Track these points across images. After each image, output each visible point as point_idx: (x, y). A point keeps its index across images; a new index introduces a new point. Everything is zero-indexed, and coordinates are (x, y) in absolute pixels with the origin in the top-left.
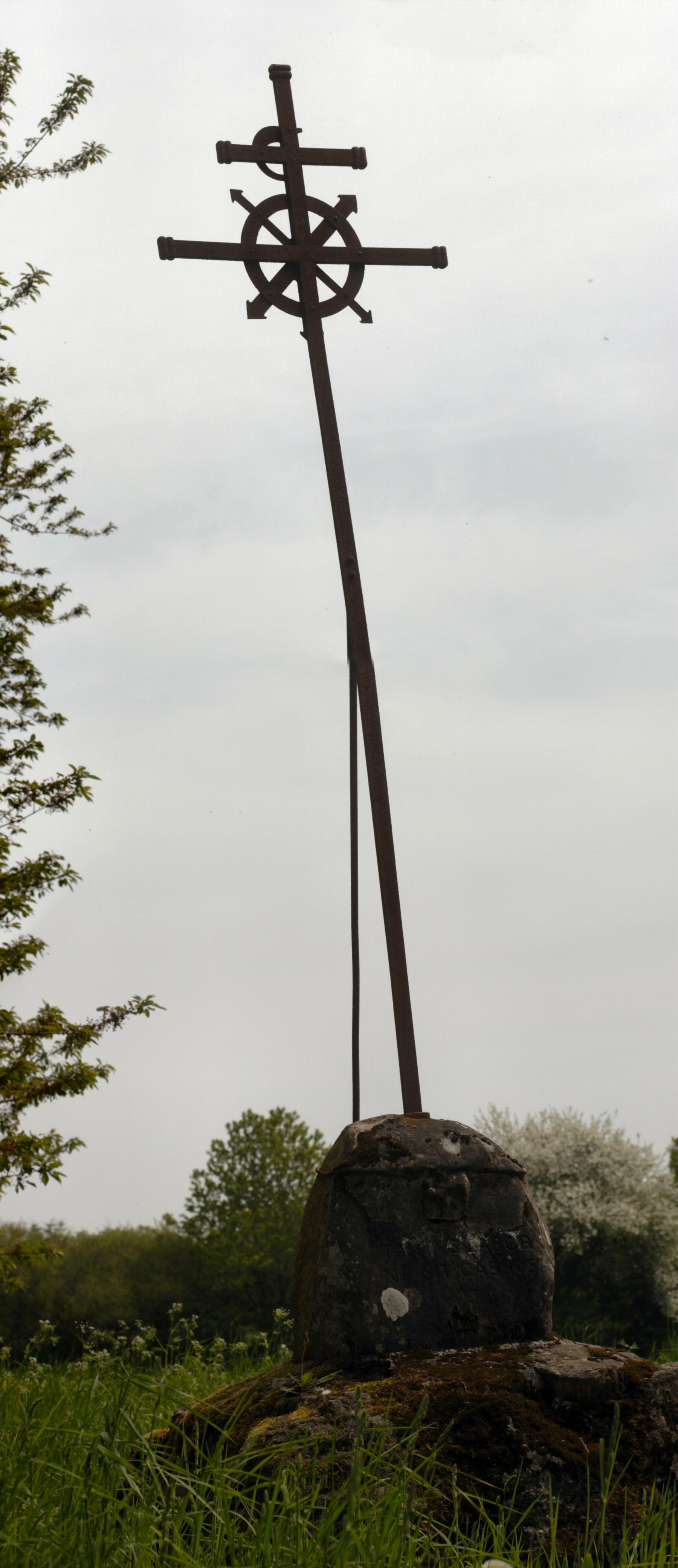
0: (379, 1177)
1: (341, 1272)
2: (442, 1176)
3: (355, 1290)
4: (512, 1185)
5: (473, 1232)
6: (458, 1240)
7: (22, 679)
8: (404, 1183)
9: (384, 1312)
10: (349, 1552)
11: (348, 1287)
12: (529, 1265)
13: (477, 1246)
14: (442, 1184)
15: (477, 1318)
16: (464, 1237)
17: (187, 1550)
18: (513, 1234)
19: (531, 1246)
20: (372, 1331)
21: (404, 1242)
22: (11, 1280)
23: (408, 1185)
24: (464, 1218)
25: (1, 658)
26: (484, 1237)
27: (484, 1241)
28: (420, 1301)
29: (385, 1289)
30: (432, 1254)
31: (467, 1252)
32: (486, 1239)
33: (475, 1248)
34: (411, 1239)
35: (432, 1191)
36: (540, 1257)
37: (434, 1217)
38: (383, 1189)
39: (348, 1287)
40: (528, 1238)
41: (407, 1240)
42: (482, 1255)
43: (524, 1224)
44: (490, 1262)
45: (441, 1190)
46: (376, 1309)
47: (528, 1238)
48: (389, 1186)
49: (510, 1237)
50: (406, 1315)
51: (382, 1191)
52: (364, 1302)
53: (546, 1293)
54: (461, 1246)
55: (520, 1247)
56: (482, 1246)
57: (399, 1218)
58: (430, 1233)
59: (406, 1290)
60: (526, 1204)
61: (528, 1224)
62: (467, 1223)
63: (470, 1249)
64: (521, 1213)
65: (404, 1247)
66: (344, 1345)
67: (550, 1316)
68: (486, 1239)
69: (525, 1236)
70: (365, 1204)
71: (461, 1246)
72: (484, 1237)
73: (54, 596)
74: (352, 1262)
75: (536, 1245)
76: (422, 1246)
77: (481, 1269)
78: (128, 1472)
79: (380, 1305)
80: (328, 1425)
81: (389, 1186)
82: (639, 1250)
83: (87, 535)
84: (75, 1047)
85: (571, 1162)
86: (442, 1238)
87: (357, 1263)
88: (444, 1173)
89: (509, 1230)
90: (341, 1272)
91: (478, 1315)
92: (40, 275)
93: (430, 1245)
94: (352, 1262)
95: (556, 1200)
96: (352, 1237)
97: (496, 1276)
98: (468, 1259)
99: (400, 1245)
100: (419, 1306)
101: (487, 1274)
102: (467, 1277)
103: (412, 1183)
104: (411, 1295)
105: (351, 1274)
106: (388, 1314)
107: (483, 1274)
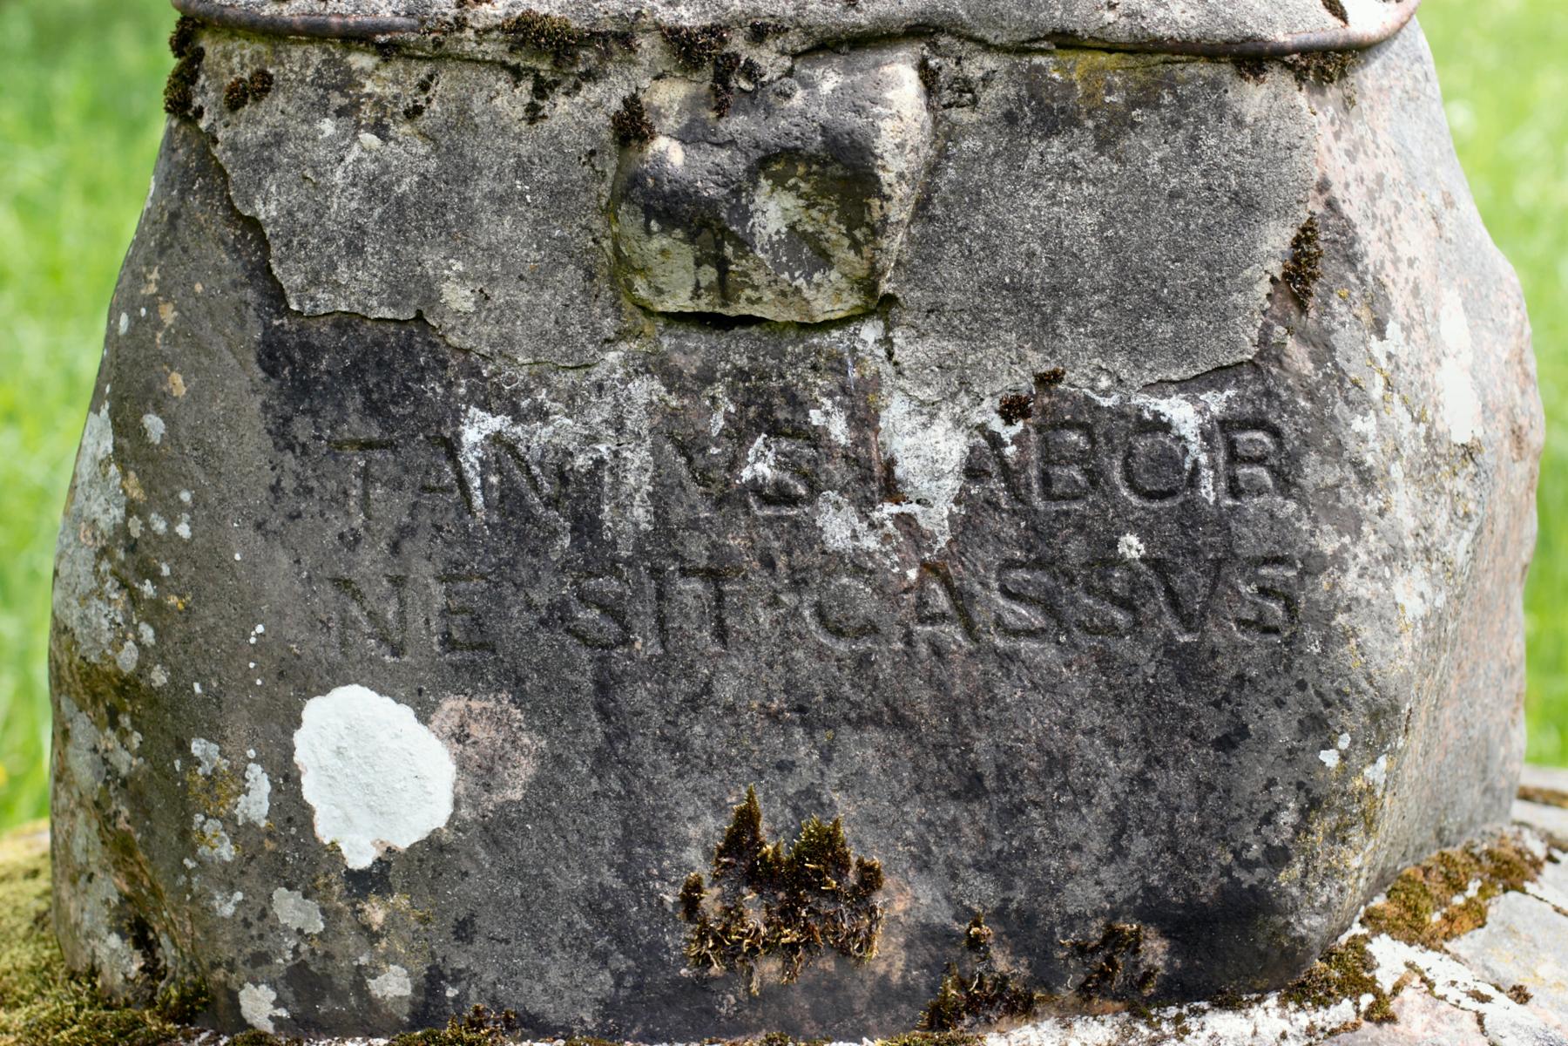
0: (361, 61)
1: (105, 566)
2: (751, 71)
3: (159, 677)
4: (1239, 123)
5: (927, 394)
6: (815, 438)
7: (798, 577)
8: (511, 100)
9: (307, 812)
10: (1222, 454)
11: (128, 658)
12: (1248, 590)
13: (937, 476)
14: (736, 124)
15: (870, 879)
16: (864, 420)
17: (1487, 749)
18: (1181, 413)
19: (1286, 483)
20: (228, 910)
21: (471, 435)
22: (947, 112)
23: (533, 114)
24: (881, 306)
25: (6, 115)
26: (997, 424)
27: (995, 441)
28: (527, 769)
29: (324, 690)
30: (641, 514)
31: (864, 505)
32: (1007, 433)
33: (924, 486)
34: (518, 417)
35: (660, 159)
36: (1328, 544)
37: (680, 301)
38: (380, 129)
39: (128, 658)
40: (1276, 433)
41: (495, 423)
42: (966, 527)
43: (1269, 352)
44: (1011, 564)
45: (723, 156)
46: (256, 801)
47: (1276, 433)
48: (414, 113)
49: (1160, 425)
50: (433, 845)
51: (369, 139)
52: (197, 747)
53: (1330, 758)
54: (837, 470)
55: (1209, 490)
56: (973, 471)
57: (458, 297)
58: (645, 389)
59: (452, 705)
60: (1306, 236)
61: (1299, 356)
62: (898, 337)
63: (891, 489)
64: (1265, 287)
65: (470, 459)
66: (114, 941)
67: (1079, 478)
68: (1007, 433)
69: (1260, 424)
70: (265, 210)
71: (837, 470)
72: (997, 424)
73: (773, 191)
74: (160, 526)
75: (1315, 472)
76: (582, 462)
77: (941, 600)
78: (1521, 542)
79: (287, 779)
80: (585, 86)
81: (414, 113)
82: (302, 429)
83: (1483, 1032)
84: (743, 227)
85: (1170, 282)
86: (718, 423)
87: (184, 530)
88: (769, 60)
89: (1160, 387)
90: (105, 566)
91: (877, 860)
92: (1372, 413)
93: (637, 457)
94: (160, 526)
95: (951, 619)
96: (177, 384)
97: (1025, 645)
98: (870, 542)
99: (451, 448)
100: (518, 795)
101: (970, 630)
102: (842, 647)
103: (561, 107)
104: (477, 731)
105: (148, 589)
106: (325, 830)
107: (952, 633)
